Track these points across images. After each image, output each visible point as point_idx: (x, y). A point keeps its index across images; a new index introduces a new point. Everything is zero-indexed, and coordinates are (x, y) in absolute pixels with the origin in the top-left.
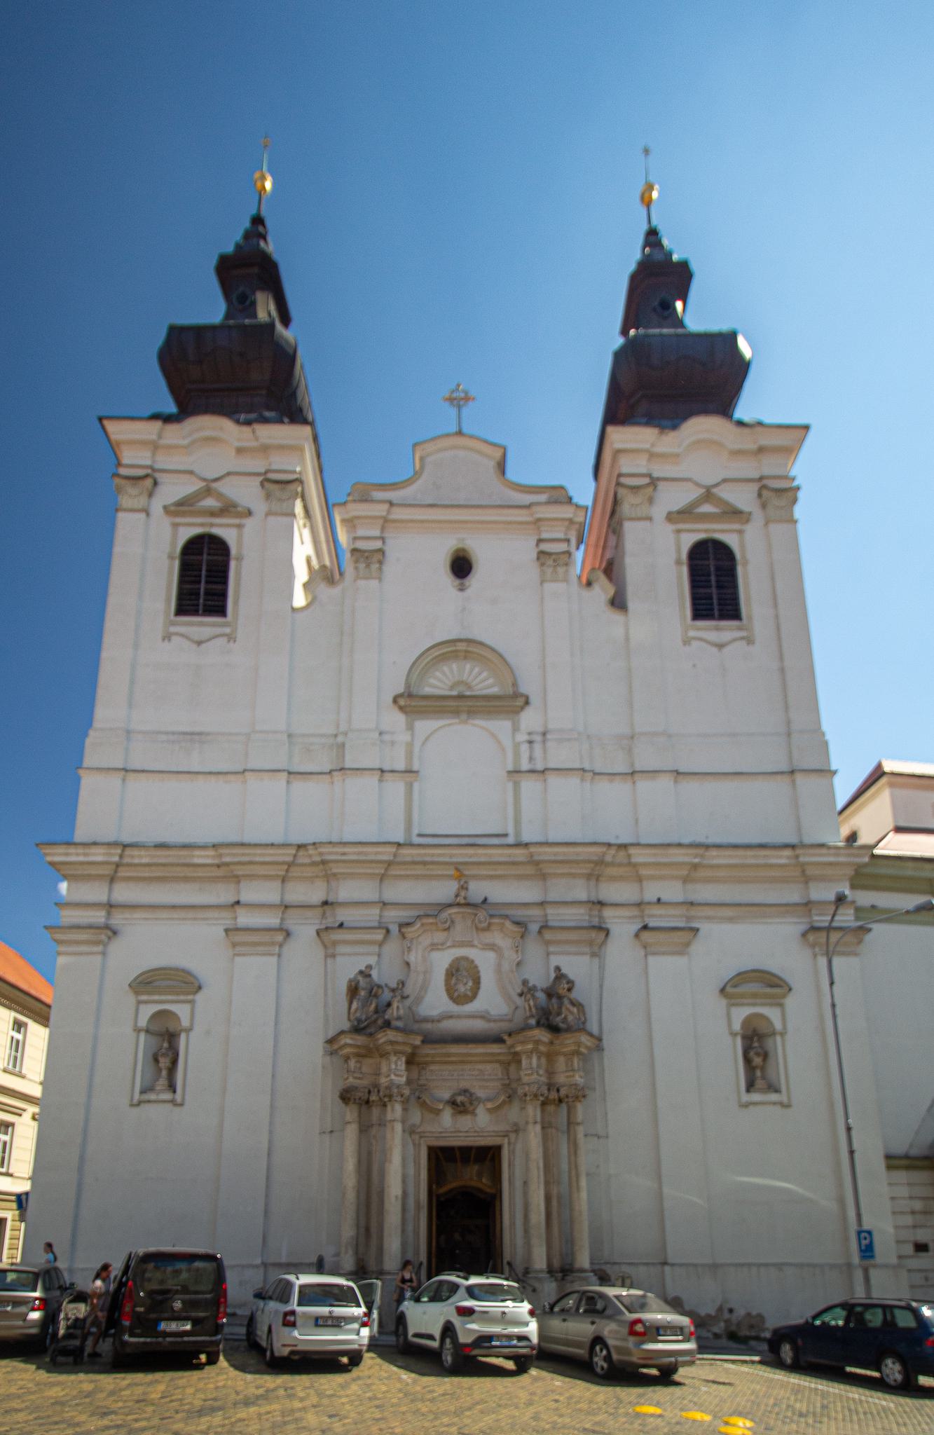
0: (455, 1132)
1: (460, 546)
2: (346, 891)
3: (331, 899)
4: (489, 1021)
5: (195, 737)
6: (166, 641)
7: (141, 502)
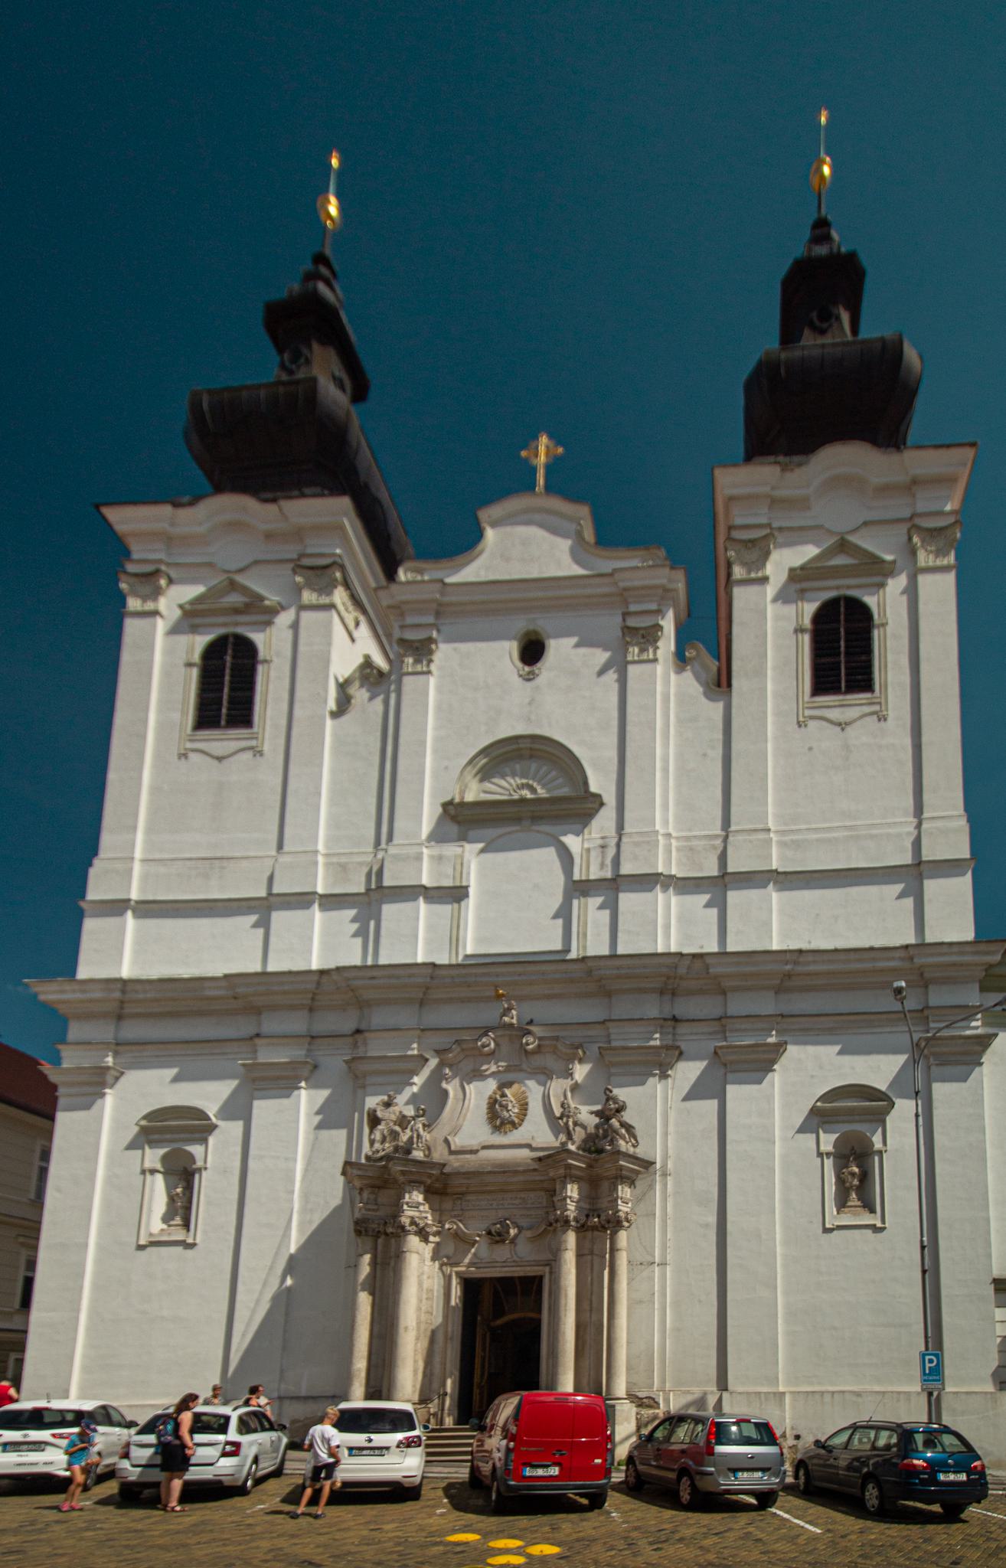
1: (531, 628)
3: (363, 1027)
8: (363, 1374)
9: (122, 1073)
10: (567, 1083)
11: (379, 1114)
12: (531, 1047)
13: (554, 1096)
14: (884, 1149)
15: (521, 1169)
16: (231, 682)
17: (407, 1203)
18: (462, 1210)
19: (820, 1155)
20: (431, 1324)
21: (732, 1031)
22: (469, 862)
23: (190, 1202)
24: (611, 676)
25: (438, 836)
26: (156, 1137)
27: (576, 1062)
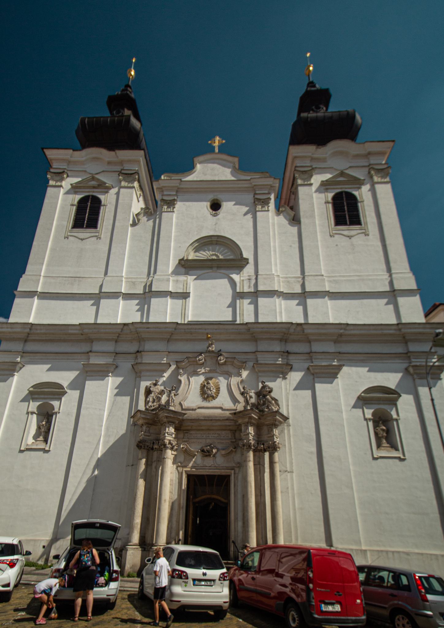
0: (204, 466)
1: (215, 198)
3: (140, 349)
6: (66, 239)
8: (139, 526)
9: (24, 366)
10: (239, 379)
11: (151, 389)
12: (222, 361)
13: (233, 385)
14: (398, 418)
15: (221, 419)
16: (89, 212)
17: (167, 433)
18: (188, 438)
19: (366, 419)
20: (172, 499)
21: (315, 359)
22: (190, 283)
23: (49, 430)
24: (249, 216)
25: (176, 272)
26: (36, 396)
27: (243, 370)
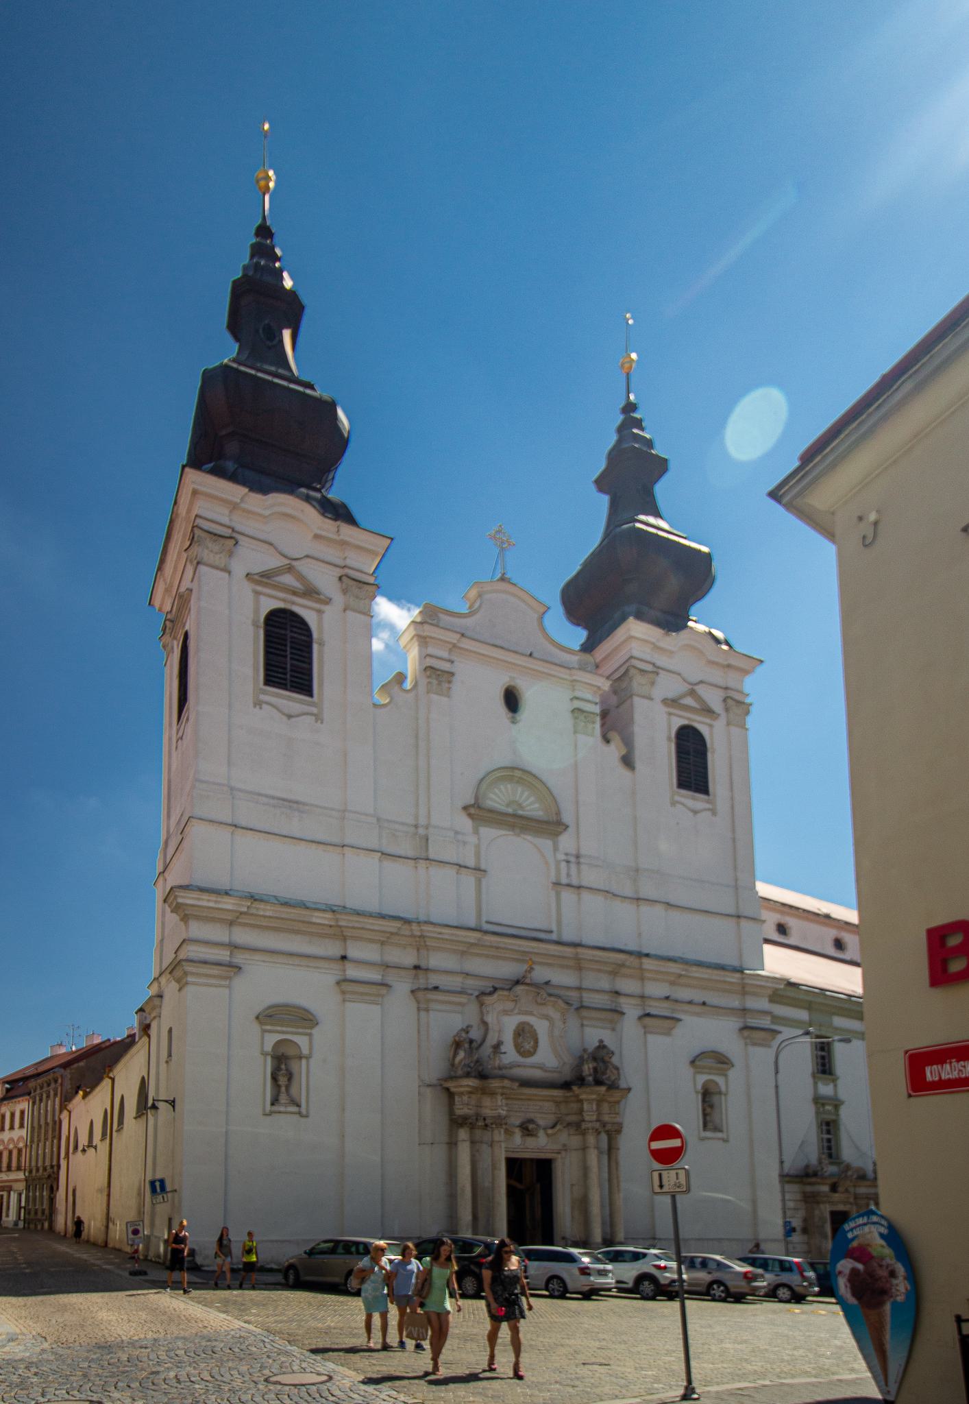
1: (512, 684)
2: (436, 960)
3: (423, 965)
4: (546, 1071)
5: (291, 805)
6: (258, 707)
7: (220, 560)
